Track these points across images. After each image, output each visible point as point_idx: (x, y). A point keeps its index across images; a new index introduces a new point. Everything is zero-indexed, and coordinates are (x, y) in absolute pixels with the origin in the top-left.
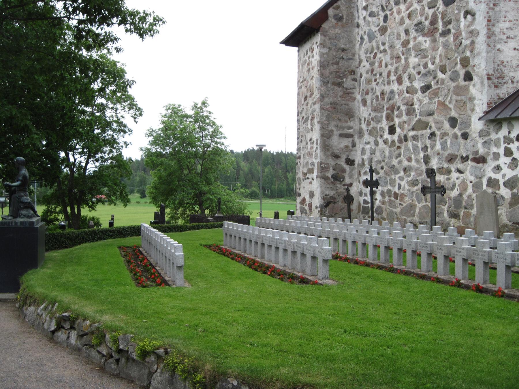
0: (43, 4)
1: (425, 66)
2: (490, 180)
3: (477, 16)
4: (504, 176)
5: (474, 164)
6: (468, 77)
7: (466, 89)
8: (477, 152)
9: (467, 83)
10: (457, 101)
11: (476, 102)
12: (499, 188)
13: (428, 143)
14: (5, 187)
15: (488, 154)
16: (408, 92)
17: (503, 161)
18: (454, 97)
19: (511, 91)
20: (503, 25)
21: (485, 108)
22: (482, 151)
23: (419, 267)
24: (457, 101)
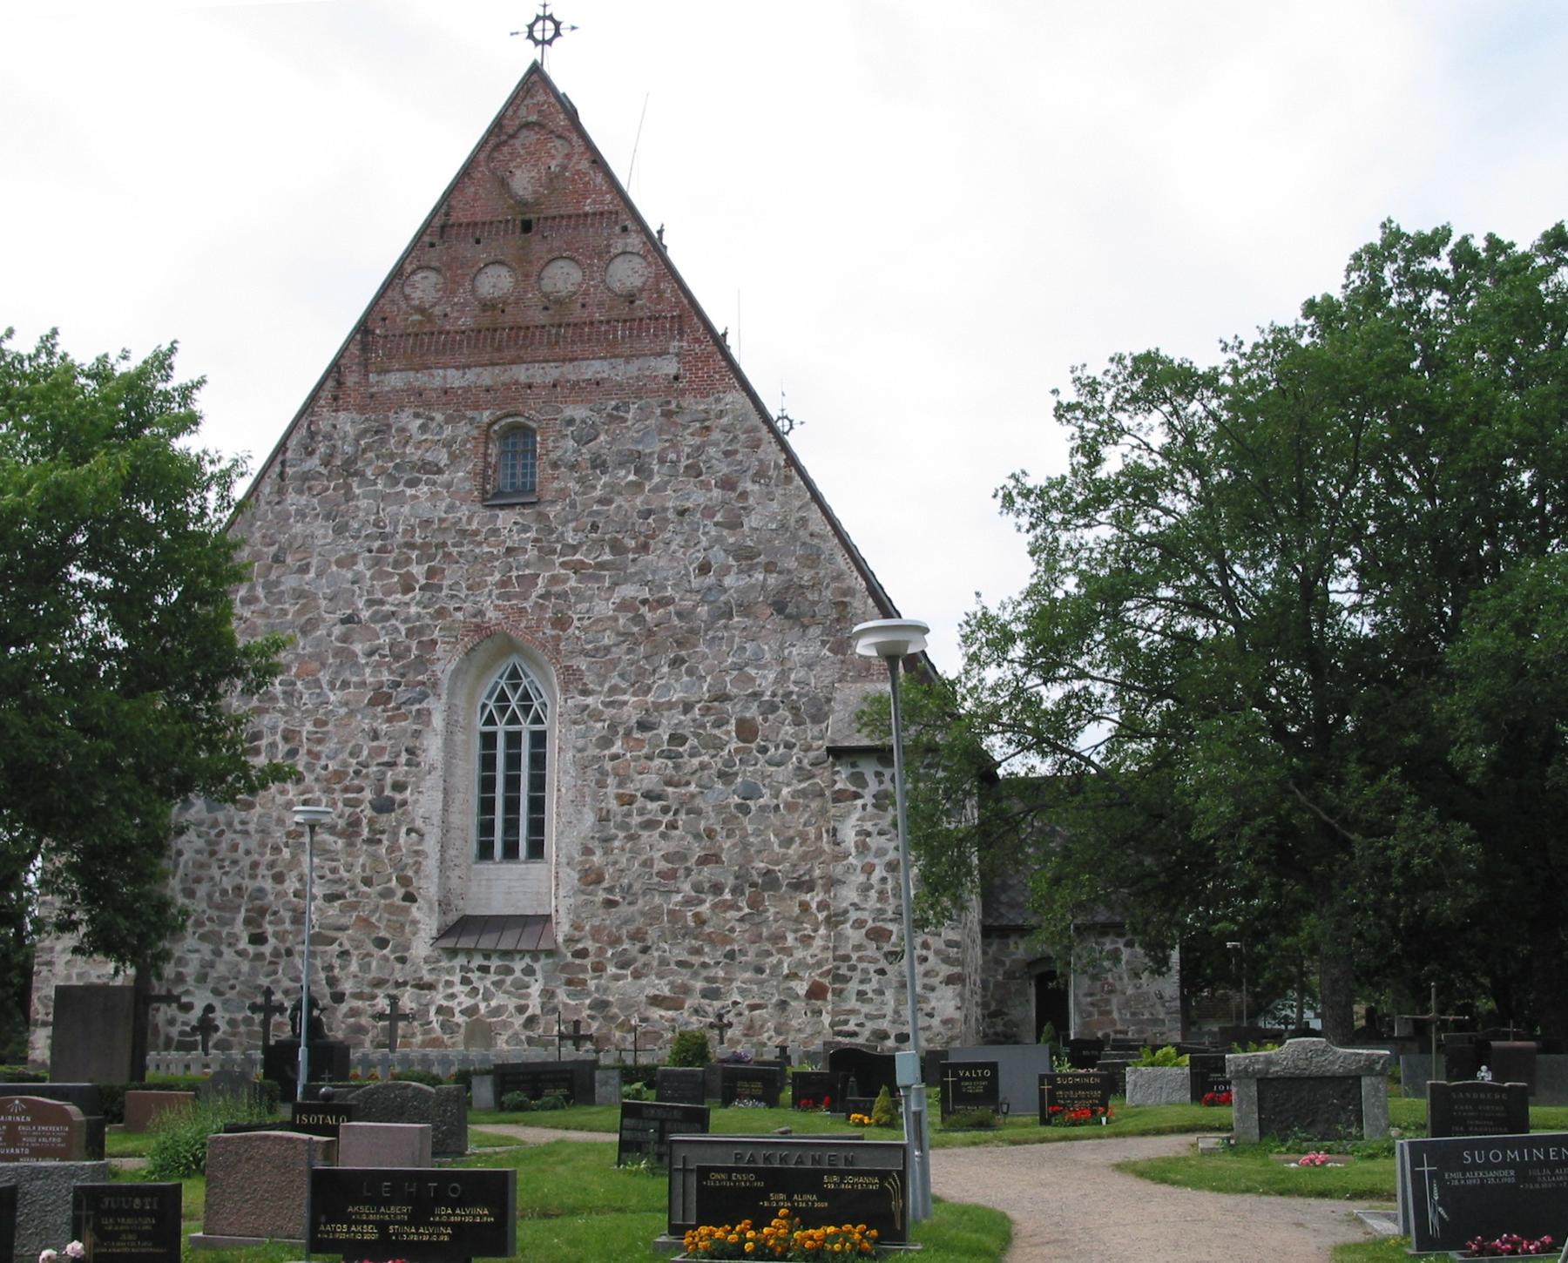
0: (126, 645)
1: (334, 870)
2: (440, 1010)
3: (427, 837)
4: (460, 1004)
5: (416, 991)
6: (410, 898)
7: (407, 911)
8: (421, 978)
9: (407, 904)
10: (389, 920)
11: (421, 926)
12: (453, 1015)
13: (337, 962)
14: (1194, 1023)
15: (438, 981)
16: (295, 896)
17: (458, 988)
18: (386, 916)
19: (456, 919)
20: (452, 852)
21: (434, 933)
22: (428, 978)
23: (601, 1086)
24: (389, 920)
